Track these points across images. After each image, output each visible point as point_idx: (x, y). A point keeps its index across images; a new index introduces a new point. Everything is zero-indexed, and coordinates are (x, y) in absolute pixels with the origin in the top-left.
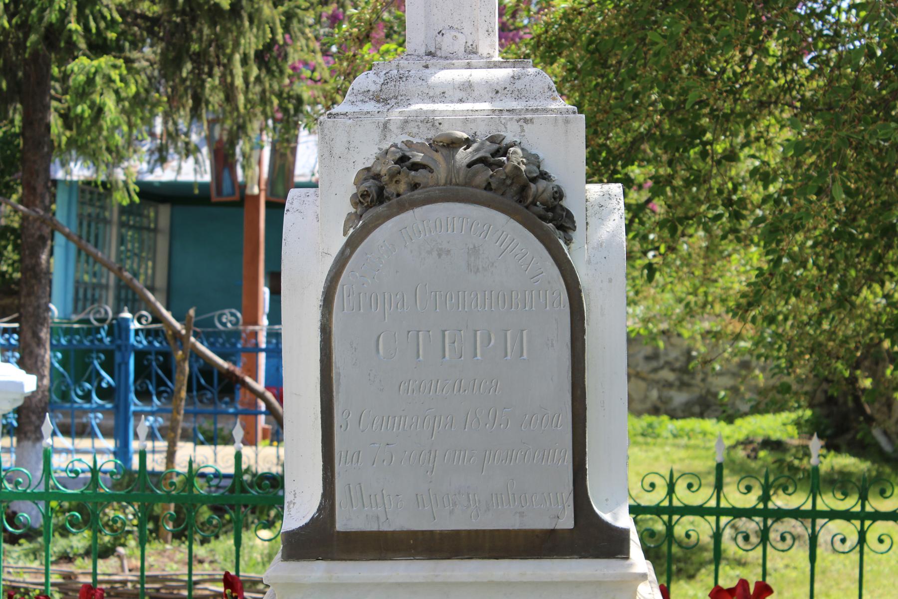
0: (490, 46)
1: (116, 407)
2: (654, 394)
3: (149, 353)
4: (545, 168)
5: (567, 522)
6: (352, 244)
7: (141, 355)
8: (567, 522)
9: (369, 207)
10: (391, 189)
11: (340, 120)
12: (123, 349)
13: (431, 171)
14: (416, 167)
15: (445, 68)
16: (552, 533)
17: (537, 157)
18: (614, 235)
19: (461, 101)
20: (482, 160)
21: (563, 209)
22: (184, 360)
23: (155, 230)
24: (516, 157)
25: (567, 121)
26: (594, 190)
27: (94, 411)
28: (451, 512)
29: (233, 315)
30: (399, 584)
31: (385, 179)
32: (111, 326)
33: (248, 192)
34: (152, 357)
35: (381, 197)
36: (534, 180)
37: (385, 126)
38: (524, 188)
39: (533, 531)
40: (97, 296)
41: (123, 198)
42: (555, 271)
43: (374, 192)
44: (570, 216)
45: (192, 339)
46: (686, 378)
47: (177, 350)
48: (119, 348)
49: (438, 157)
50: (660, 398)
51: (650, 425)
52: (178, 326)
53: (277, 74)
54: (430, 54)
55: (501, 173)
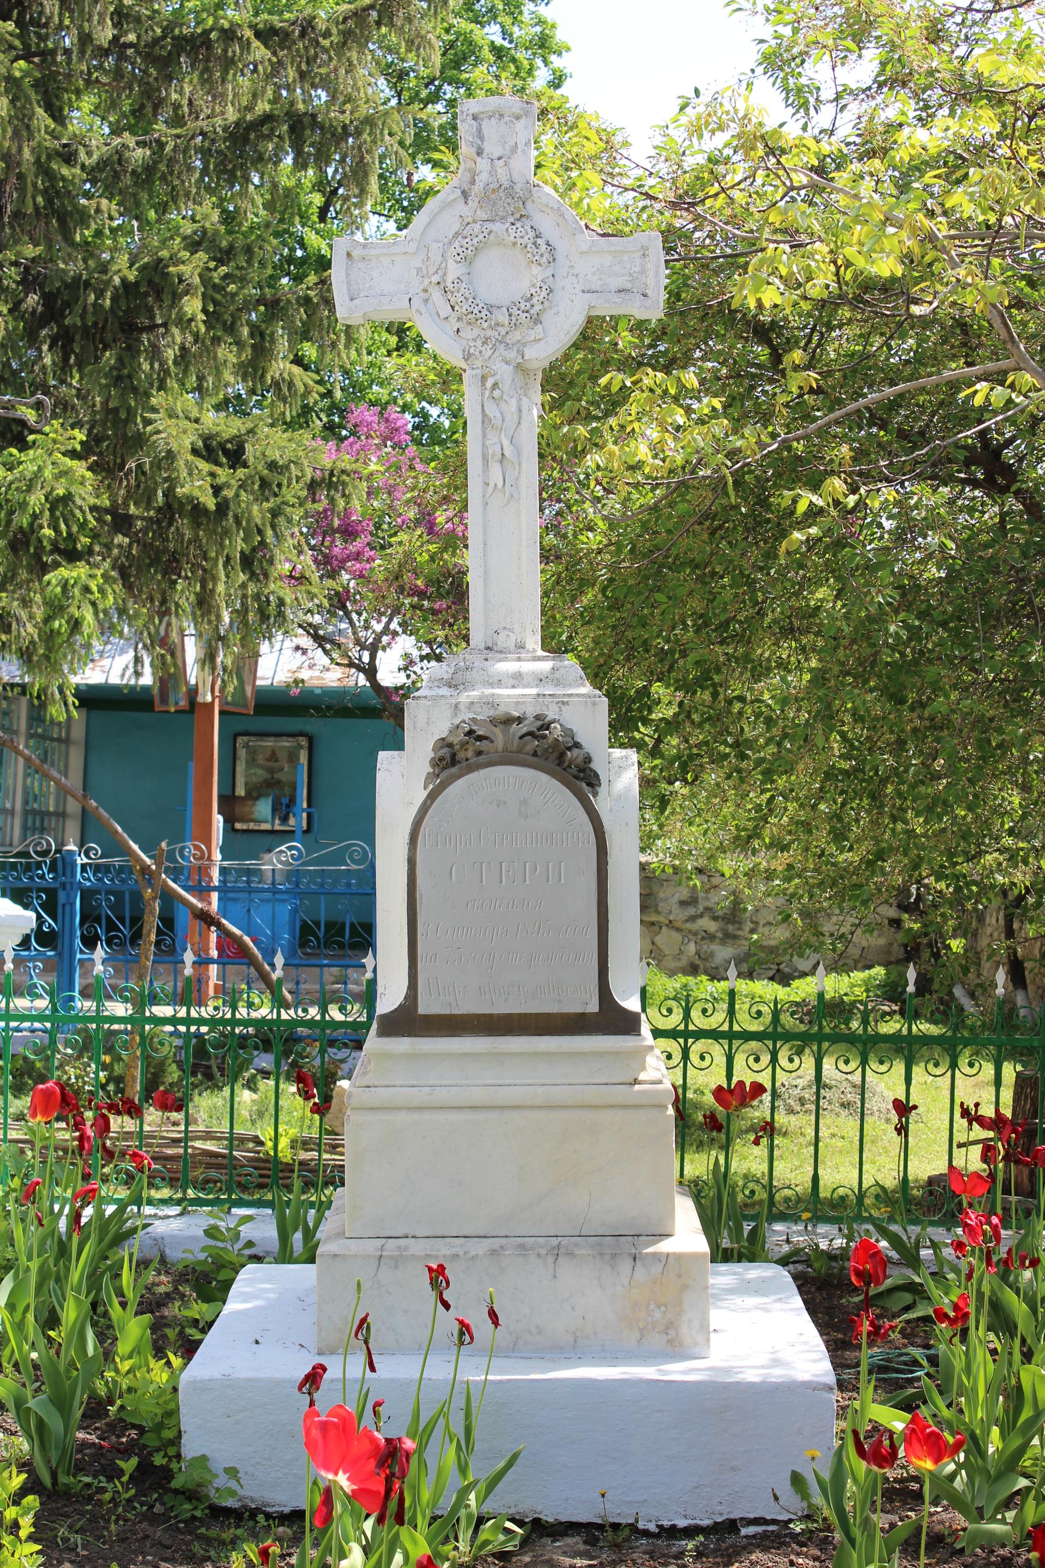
0: (534, 642)
1: (60, 955)
2: (692, 948)
3: (99, 892)
4: (578, 739)
5: (593, 1007)
6: (432, 797)
7: (87, 895)
8: (593, 1007)
9: (444, 769)
10: (461, 755)
11: (422, 701)
12: (68, 886)
13: (492, 742)
14: (480, 738)
15: (500, 660)
16: (582, 1015)
17: (571, 730)
18: (628, 789)
19: (513, 687)
20: (530, 734)
21: (592, 770)
22: (154, 899)
23: (67, 741)
24: (557, 730)
25: (594, 704)
26: (617, 753)
27: (32, 959)
28: (506, 1000)
29: (197, 847)
30: (466, 1055)
31: (457, 747)
32: (54, 862)
33: (200, 699)
34: (102, 897)
35: (453, 761)
36: (569, 749)
37: (456, 706)
38: (562, 755)
39: (568, 1014)
40: (46, 825)
41: (60, 713)
42: (585, 818)
43: (448, 759)
44: (596, 775)
45: (164, 876)
46: (730, 928)
47: (146, 888)
48: (63, 885)
49: (497, 731)
50: (698, 953)
51: (685, 986)
52: (148, 861)
53: (261, 577)
54: (488, 648)
55: (545, 744)
